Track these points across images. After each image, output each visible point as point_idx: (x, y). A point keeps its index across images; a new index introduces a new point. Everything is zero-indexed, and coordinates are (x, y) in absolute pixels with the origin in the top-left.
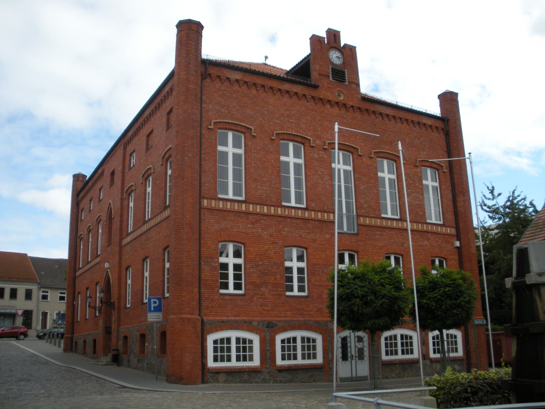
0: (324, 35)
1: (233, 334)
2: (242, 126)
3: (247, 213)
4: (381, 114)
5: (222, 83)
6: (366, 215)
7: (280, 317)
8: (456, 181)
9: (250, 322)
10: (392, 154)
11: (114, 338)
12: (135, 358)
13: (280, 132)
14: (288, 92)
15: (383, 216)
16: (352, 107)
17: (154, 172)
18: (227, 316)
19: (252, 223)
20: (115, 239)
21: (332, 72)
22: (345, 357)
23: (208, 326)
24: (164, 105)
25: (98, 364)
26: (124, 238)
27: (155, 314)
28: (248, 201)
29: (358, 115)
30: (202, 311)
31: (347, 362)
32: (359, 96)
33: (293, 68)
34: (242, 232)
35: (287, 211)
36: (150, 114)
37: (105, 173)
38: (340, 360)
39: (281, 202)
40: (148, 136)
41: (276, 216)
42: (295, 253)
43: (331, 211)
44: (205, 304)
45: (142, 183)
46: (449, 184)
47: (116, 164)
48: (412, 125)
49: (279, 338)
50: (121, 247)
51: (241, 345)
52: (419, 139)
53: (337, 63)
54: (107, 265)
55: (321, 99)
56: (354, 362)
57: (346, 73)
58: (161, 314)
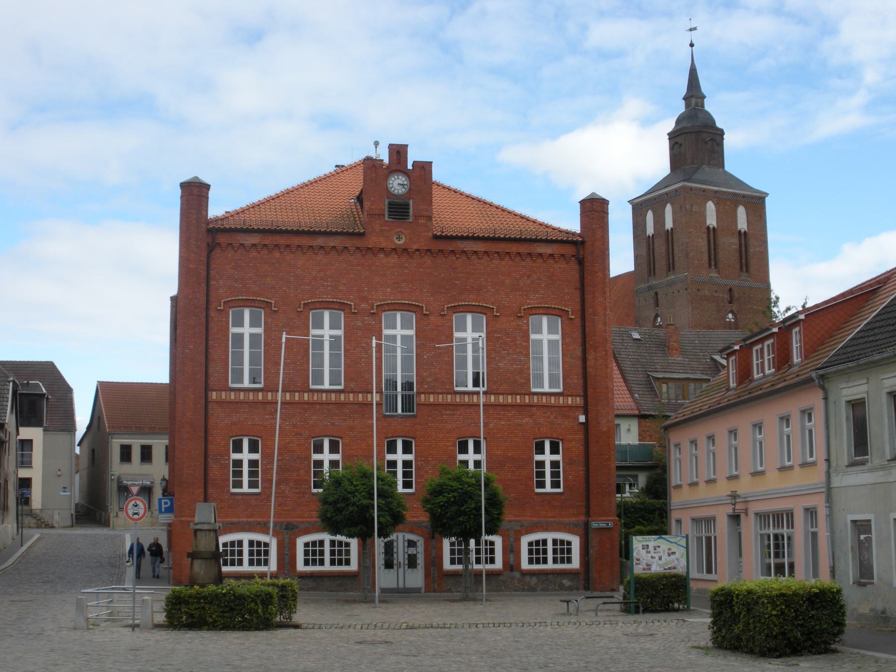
1: (550, 536)
5: (236, 251)
16: (418, 250)
22: (389, 565)
29: (428, 260)
31: (392, 570)
32: (430, 234)
41: (301, 403)
49: (300, 542)
51: (255, 548)
52: (529, 276)
53: (400, 192)
56: (401, 570)
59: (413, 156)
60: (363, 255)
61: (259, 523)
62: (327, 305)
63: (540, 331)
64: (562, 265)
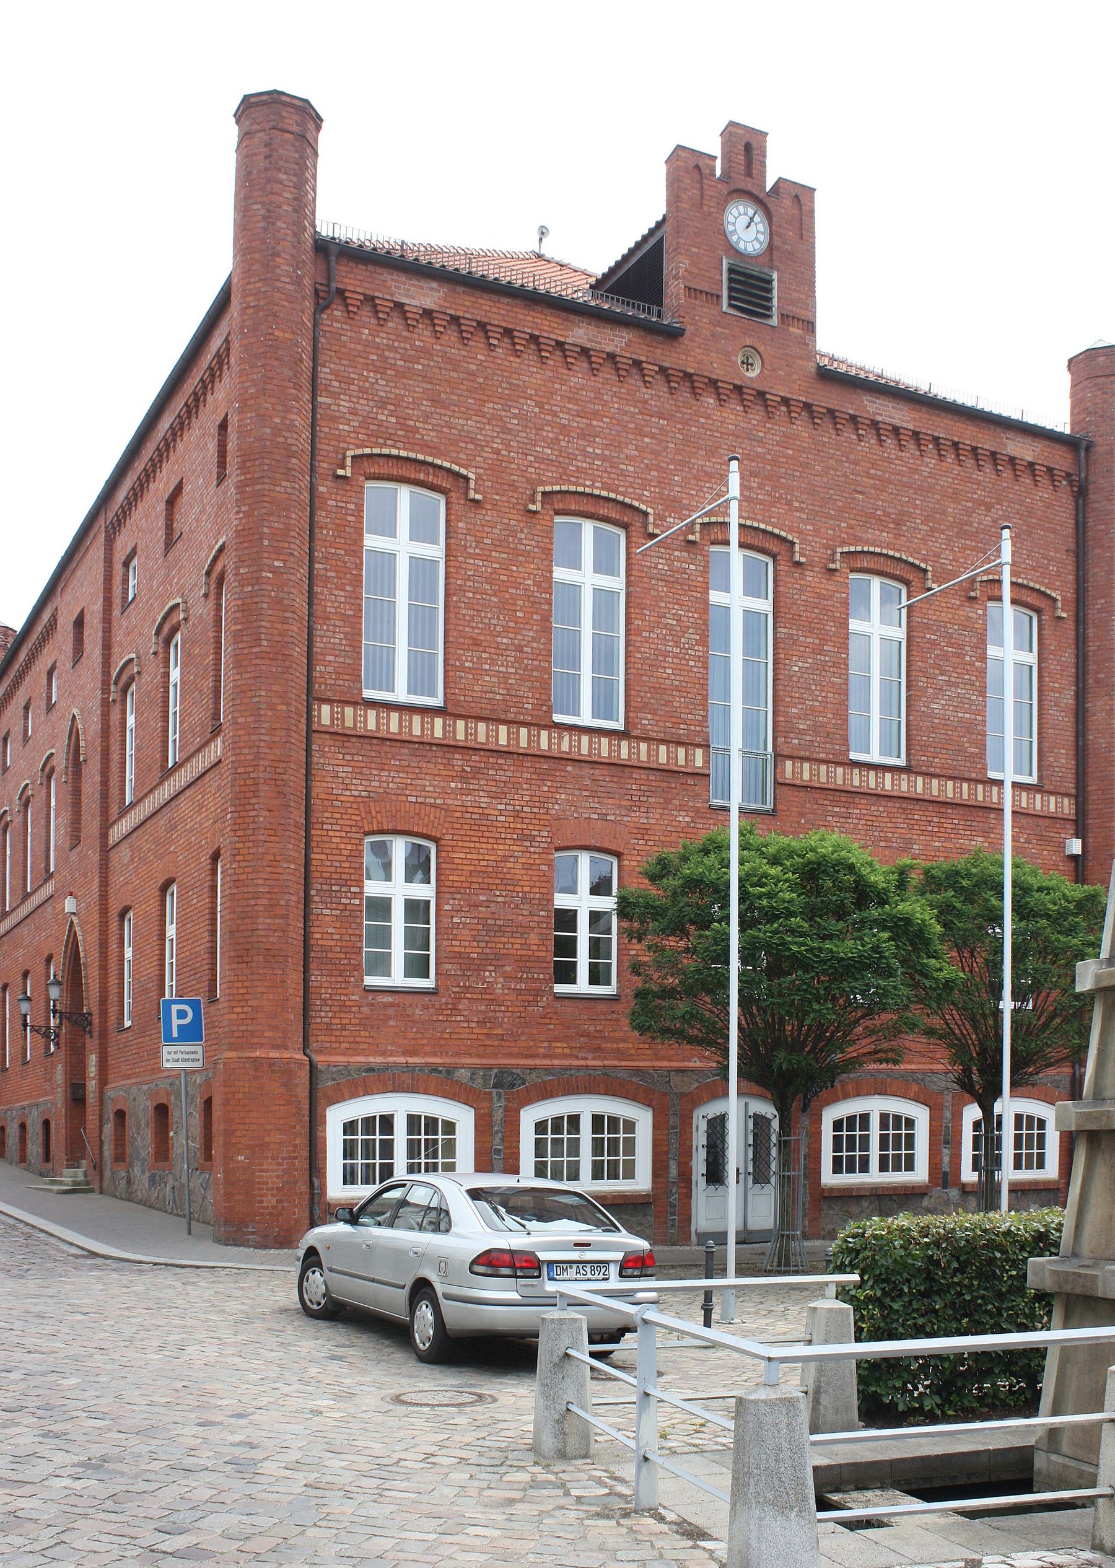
0: (713, 146)
2: (441, 467)
3: (449, 747)
4: (875, 425)
5: (381, 322)
6: (802, 753)
7: (532, 1056)
8: (1092, 647)
9: (450, 1070)
10: (899, 559)
11: (92, 1117)
12: (143, 1172)
13: (557, 488)
14: (585, 352)
15: (854, 756)
16: (785, 401)
17: (186, 619)
18: (384, 1053)
19: (463, 777)
20: (91, 825)
21: (730, 280)
23: (330, 1083)
24: (210, 398)
25: (51, 1191)
26: (114, 823)
27: (183, 1048)
28: (450, 709)
29: (801, 427)
30: (312, 1039)
33: (612, 271)
34: (431, 805)
35: (566, 738)
36: (171, 427)
37: (61, 620)
38: (702, 1182)
39: (549, 712)
40: (171, 502)
42: (585, 866)
43: (698, 740)
44: (322, 1017)
45: (155, 653)
46: (1068, 656)
47: (84, 594)
48: (970, 463)
50: (106, 851)
53: (750, 249)
54: (70, 904)
55: (688, 376)
57: (775, 284)
58: (199, 1049)
59: (778, 167)
60: (672, 391)
61: (435, 1070)
62: (591, 507)
63: (575, 563)
64: (1044, 493)
